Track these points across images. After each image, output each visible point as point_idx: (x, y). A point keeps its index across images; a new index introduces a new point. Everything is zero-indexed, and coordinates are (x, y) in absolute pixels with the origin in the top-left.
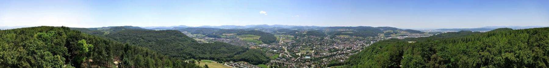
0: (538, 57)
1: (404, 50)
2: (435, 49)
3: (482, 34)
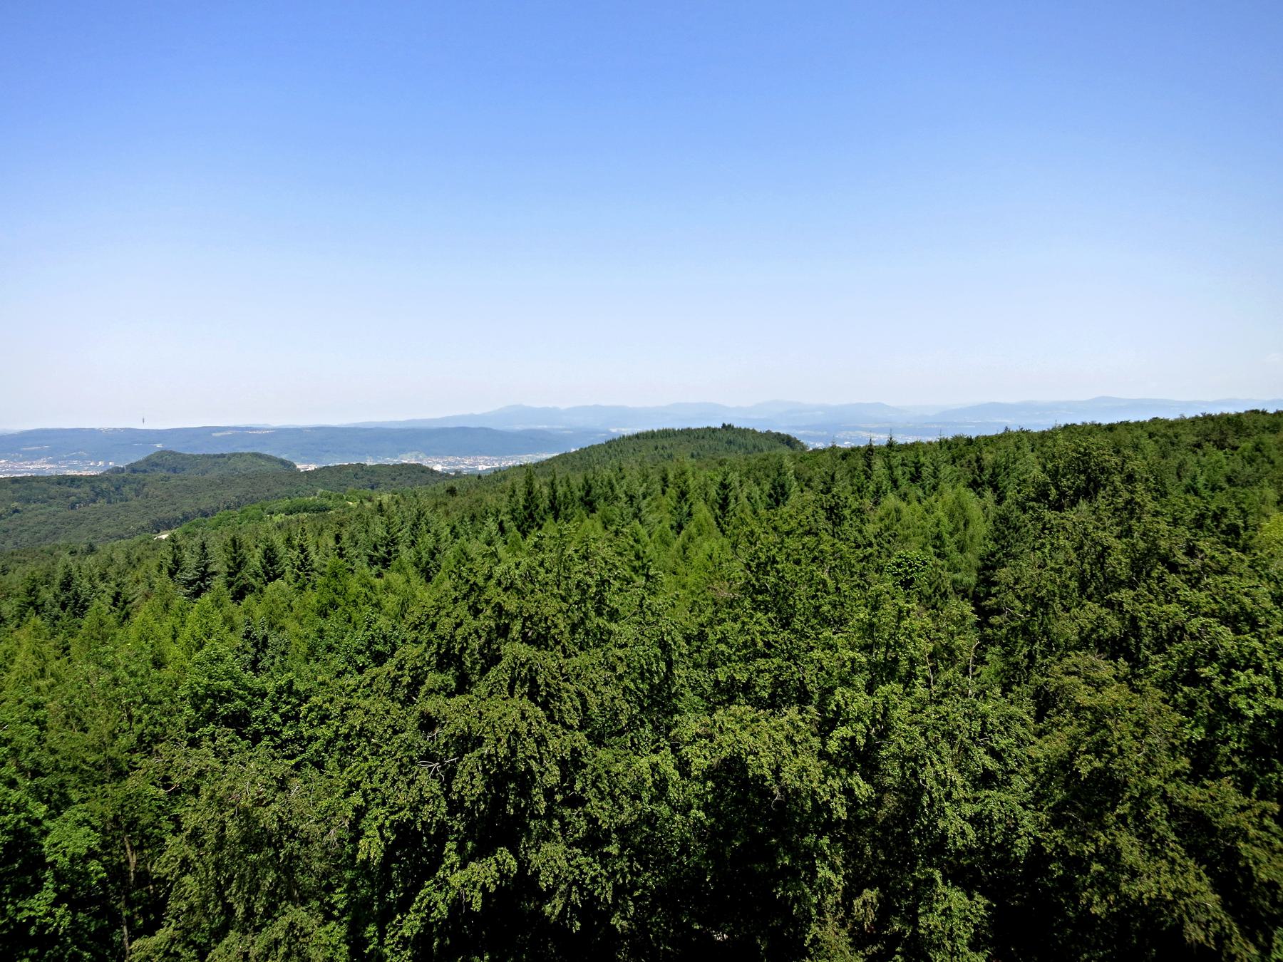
0: (1106, 787)
3: (452, 487)
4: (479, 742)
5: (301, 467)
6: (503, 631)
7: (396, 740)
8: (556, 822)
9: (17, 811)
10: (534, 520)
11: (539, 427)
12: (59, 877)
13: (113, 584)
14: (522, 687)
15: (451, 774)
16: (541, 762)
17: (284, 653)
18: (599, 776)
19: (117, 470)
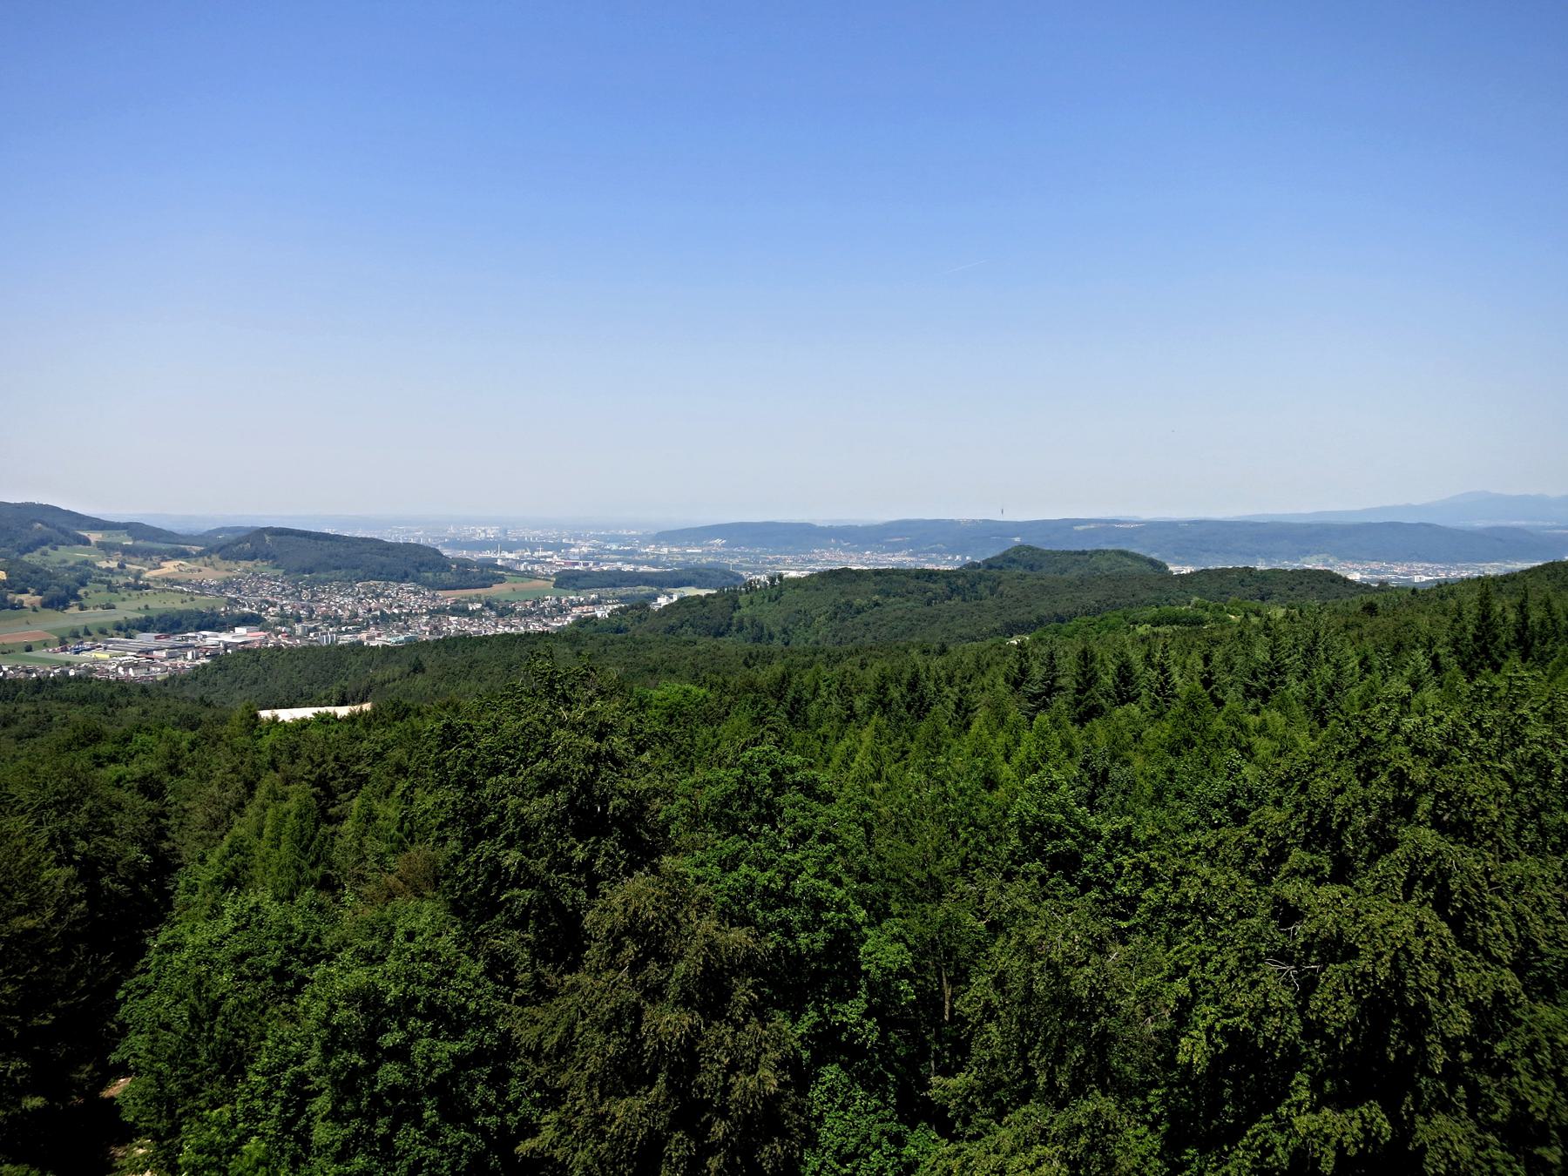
1: (186, 844)
2: (639, 804)
3: (1373, 602)
4: (1352, 952)
5: (1174, 569)
6: (1406, 809)
7: (1241, 925)
8: (1461, 1089)
9: (839, 911)
10: (1489, 656)
11: (1514, 523)
12: (872, 989)
13: (956, 690)
14: (1425, 889)
15: (1308, 986)
16: (1441, 997)
17: (1124, 792)
18: (1536, 1042)
19: (974, 566)
